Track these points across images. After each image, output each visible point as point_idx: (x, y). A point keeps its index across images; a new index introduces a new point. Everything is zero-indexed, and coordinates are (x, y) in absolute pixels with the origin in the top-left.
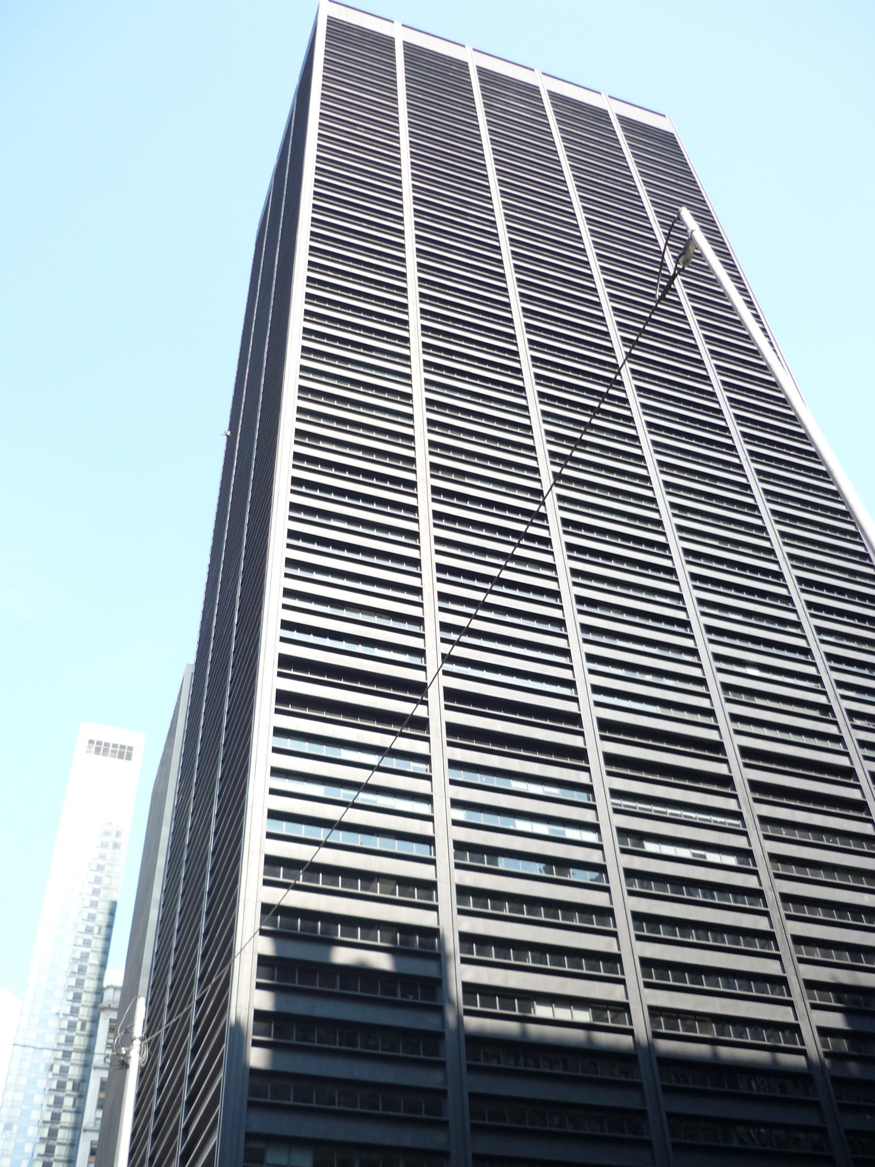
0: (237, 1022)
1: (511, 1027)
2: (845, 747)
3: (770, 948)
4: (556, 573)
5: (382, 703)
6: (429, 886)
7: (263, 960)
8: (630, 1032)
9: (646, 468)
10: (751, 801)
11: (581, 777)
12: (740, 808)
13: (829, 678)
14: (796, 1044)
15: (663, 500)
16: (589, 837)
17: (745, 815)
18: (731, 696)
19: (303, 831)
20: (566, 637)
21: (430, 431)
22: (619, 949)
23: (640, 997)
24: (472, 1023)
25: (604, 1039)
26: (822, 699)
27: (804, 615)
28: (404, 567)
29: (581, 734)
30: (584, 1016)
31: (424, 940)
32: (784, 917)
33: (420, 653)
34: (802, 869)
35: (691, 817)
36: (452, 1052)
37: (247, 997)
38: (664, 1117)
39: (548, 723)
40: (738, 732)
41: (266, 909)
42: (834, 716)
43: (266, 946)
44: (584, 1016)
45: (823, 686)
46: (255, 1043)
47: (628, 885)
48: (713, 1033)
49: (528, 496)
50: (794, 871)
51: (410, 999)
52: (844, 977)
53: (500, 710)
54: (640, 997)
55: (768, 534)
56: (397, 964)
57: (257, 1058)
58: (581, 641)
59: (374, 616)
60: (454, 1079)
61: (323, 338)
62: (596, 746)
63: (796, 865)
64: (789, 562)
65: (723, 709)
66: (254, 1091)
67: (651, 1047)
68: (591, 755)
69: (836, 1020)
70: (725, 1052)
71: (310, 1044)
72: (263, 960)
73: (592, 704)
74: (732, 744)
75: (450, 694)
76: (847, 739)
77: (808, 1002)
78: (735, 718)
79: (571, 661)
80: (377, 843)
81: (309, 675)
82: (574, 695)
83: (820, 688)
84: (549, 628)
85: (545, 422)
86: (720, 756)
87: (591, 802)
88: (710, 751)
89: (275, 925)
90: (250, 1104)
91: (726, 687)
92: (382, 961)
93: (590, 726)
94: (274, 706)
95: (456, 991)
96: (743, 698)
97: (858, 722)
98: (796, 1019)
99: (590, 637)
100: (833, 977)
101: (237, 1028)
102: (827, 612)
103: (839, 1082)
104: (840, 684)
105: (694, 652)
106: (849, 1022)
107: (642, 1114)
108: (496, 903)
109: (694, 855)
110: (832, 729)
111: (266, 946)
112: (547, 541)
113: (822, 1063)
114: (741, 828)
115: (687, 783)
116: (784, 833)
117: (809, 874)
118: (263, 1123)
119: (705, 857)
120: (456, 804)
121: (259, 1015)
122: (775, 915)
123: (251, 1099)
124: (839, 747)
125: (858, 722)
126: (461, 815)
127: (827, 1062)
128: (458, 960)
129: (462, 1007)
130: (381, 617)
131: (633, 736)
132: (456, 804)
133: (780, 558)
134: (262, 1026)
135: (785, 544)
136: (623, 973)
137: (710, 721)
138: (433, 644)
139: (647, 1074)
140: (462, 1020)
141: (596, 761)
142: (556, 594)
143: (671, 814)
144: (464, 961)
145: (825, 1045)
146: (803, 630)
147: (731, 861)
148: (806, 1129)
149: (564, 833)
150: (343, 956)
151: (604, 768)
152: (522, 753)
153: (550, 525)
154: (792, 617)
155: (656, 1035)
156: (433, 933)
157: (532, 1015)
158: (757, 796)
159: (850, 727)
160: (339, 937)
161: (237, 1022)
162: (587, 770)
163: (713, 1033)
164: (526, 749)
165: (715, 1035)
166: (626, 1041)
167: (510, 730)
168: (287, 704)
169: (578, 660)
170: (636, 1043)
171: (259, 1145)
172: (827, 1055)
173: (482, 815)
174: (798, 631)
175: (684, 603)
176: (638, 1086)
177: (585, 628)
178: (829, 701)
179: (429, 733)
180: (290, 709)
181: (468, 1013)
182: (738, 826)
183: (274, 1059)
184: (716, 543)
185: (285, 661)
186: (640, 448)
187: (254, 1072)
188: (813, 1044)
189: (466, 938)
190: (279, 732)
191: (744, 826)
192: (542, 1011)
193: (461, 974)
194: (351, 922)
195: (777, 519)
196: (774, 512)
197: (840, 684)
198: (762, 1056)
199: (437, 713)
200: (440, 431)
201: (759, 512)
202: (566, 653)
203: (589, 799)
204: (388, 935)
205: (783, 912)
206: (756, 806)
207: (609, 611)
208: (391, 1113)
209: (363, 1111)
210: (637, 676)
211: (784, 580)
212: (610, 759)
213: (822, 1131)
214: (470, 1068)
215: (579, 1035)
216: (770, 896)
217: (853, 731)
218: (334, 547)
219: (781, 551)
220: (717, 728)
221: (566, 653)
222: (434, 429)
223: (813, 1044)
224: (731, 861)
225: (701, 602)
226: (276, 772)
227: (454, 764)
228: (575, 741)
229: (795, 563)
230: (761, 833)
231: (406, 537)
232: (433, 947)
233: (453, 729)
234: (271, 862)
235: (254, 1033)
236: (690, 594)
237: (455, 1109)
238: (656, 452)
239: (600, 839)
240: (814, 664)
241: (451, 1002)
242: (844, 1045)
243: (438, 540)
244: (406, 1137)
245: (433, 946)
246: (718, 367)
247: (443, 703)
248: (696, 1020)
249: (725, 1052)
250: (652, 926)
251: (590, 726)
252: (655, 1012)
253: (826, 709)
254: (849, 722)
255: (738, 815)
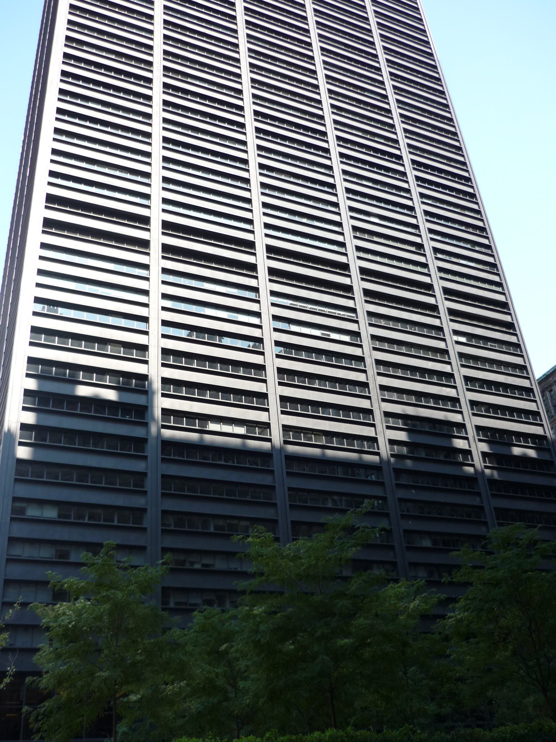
0: (9, 430)
1: (194, 436)
2: (429, 271)
3: (365, 393)
4: (247, 148)
5: (120, 229)
6: (144, 348)
7: (28, 393)
8: (269, 440)
9: (317, 79)
10: (363, 301)
11: (252, 282)
12: (355, 306)
13: (424, 226)
14: (375, 449)
15: (326, 101)
16: (254, 320)
17: (358, 310)
18: (358, 234)
19: (98, 318)
20: (249, 190)
21: (164, 43)
22: (267, 391)
23: (276, 419)
24: (167, 433)
25: (252, 443)
26: (418, 240)
27: (413, 185)
28: (140, 138)
29: (254, 254)
30: (241, 430)
31: (72, 372)
32: (376, 374)
33: (147, 197)
34: (382, 343)
35: (324, 311)
36: (153, 451)
37: (17, 415)
38: (286, 489)
39: (329, 269)
40: (359, 258)
41: (31, 361)
42: (424, 251)
43: (32, 384)
44: (241, 430)
45: (420, 232)
46: (21, 444)
47: (377, 369)
48: (323, 441)
49: (232, 94)
50: (386, 346)
51: (127, 418)
52: (411, 411)
53: (180, 232)
54: (276, 419)
55: (395, 130)
56: (120, 397)
57: (23, 453)
58: (260, 194)
59: (116, 170)
60: (153, 466)
61: (372, 69)
62: (262, 261)
63: (388, 343)
64: (407, 150)
65: (351, 242)
66: (18, 472)
67: (281, 449)
68: (260, 268)
69: (402, 436)
70: (330, 453)
71: (208, 462)
72: (28, 393)
73: (263, 235)
74: (355, 265)
75: (166, 225)
76: (431, 266)
77: (384, 425)
78: (358, 249)
79: (252, 207)
80: (110, 320)
81: (338, 271)
82: (252, 229)
83: (418, 233)
84: (239, 184)
85: (248, 42)
86: (347, 273)
87: (258, 299)
88: (340, 269)
89: (119, 383)
90: (16, 480)
91: (355, 229)
92: (111, 395)
93: (260, 250)
94: (161, 254)
95: (158, 413)
96: (366, 236)
97: (439, 256)
98: (376, 434)
99: (267, 191)
100: (403, 411)
101: (10, 435)
102: (443, 188)
103: (398, 472)
104: (431, 231)
105: (336, 205)
106: (410, 437)
107: (273, 488)
108: (188, 360)
109: (322, 334)
110: (422, 259)
111: (32, 384)
112: (327, 151)
113: (389, 460)
114: (355, 319)
115: (78, 236)
116: (383, 323)
117: (395, 348)
118: (24, 491)
119: (329, 335)
120: (165, 296)
121: (24, 427)
122: (460, 387)
123: (17, 477)
124: (425, 271)
125: (439, 256)
126: (169, 304)
127: (392, 460)
128: (160, 395)
129: (161, 423)
130: (122, 172)
131: (371, 276)
132: (165, 296)
133: (402, 147)
134: (27, 433)
135: (406, 137)
136: (268, 405)
137: (342, 250)
138: (156, 191)
139: (278, 465)
140: (160, 431)
141: (358, 294)
142: (333, 186)
143: (311, 308)
144: (163, 395)
145: (392, 450)
146: (411, 195)
147: (347, 338)
148: (377, 498)
149: (237, 317)
150: (83, 391)
151: (364, 298)
152: (213, 265)
153: (246, 114)
154: (405, 185)
155: (286, 442)
156: (144, 378)
157: (207, 429)
158: (452, 318)
159: (434, 258)
160: (81, 379)
161: (9, 430)
162: (256, 278)
163: (323, 441)
164: (216, 263)
165: (324, 443)
166: (267, 445)
167: (207, 250)
168: (51, 228)
169: (256, 206)
170: (273, 447)
171: (23, 505)
172: (392, 455)
173: (183, 304)
174: (408, 195)
175: (333, 173)
176: (272, 472)
177: (263, 185)
178: (422, 241)
179: (150, 250)
180: (53, 231)
181: (164, 427)
182: (354, 317)
183: (34, 454)
184: (360, 134)
185: (50, 198)
186: (314, 65)
187: (20, 462)
188: (384, 449)
189: (165, 381)
190: (44, 246)
191: (357, 317)
192: (213, 427)
193: (162, 403)
194: (89, 370)
195: (403, 120)
196: (402, 115)
197: (431, 231)
198: (316, 451)
199: (156, 237)
200: (173, 44)
201: (392, 115)
202: (340, 224)
203: (256, 297)
204: (115, 379)
205: (376, 371)
206: (451, 324)
207: (290, 177)
208: (125, 488)
209: (215, 496)
210: (297, 218)
211: (403, 161)
212: (272, 271)
213: (384, 499)
214: (163, 460)
215: (238, 441)
216: (368, 361)
217: (435, 261)
218: (183, 147)
219: (403, 142)
220: (346, 255)
221: (340, 224)
222: (168, 42)
223: (384, 449)
224: (347, 338)
225: (345, 172)
226: (41, 272)
227: (165, 271)
228: (346, 281)
229: (411, 150)
230: (367, 322)
231: (143, 118)
232: (144, 386)
233: (166, 248)
234: (35, 330)
235: (20, 438)
236: (338, 166)
237: (152, 484)
238: (325, 68)
239: (261, 322)
240: (416, 217)
241: (153, 419)
242: (404, 450)
243: (165, 120)
244: (120, 500)
245: (144, 386)
246: (375, 12)
247: (265, 254)
248: (313, 434)
249: (330, 453)
250: (332, 384)
251: (260, 250)
252: (286, 428)
253: (420, 246)
254: (433, 256)
255: (354, 310)
